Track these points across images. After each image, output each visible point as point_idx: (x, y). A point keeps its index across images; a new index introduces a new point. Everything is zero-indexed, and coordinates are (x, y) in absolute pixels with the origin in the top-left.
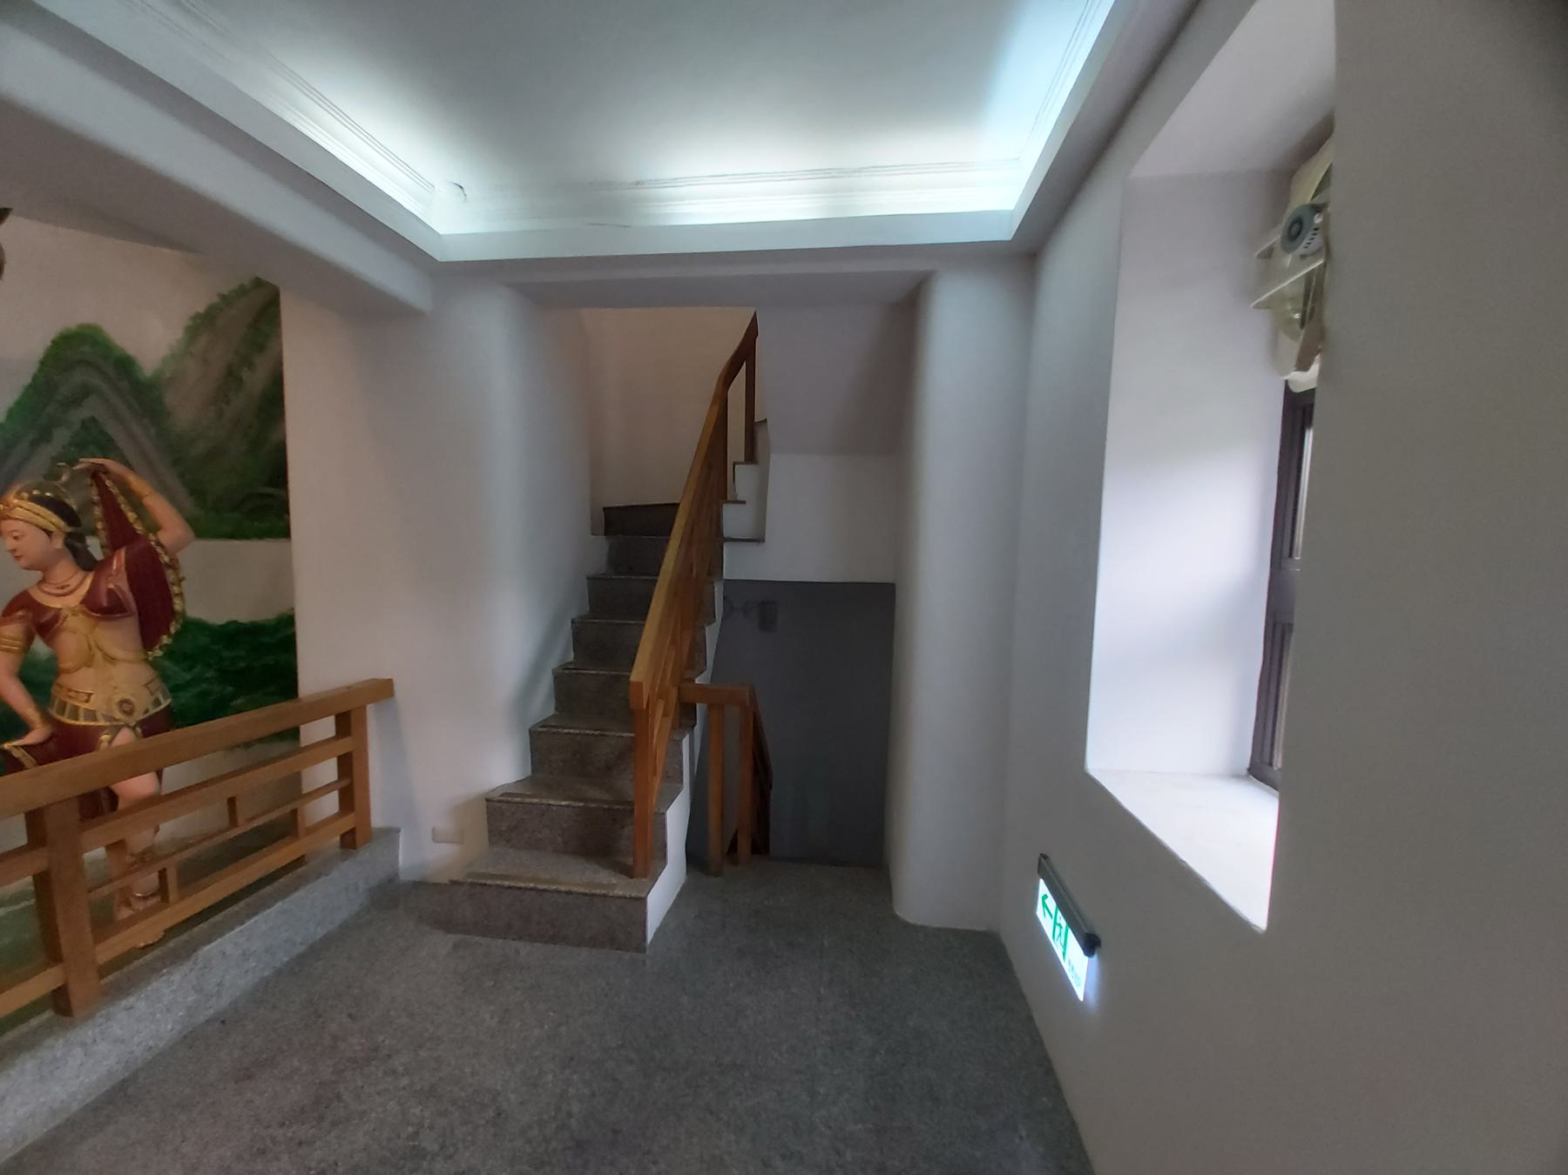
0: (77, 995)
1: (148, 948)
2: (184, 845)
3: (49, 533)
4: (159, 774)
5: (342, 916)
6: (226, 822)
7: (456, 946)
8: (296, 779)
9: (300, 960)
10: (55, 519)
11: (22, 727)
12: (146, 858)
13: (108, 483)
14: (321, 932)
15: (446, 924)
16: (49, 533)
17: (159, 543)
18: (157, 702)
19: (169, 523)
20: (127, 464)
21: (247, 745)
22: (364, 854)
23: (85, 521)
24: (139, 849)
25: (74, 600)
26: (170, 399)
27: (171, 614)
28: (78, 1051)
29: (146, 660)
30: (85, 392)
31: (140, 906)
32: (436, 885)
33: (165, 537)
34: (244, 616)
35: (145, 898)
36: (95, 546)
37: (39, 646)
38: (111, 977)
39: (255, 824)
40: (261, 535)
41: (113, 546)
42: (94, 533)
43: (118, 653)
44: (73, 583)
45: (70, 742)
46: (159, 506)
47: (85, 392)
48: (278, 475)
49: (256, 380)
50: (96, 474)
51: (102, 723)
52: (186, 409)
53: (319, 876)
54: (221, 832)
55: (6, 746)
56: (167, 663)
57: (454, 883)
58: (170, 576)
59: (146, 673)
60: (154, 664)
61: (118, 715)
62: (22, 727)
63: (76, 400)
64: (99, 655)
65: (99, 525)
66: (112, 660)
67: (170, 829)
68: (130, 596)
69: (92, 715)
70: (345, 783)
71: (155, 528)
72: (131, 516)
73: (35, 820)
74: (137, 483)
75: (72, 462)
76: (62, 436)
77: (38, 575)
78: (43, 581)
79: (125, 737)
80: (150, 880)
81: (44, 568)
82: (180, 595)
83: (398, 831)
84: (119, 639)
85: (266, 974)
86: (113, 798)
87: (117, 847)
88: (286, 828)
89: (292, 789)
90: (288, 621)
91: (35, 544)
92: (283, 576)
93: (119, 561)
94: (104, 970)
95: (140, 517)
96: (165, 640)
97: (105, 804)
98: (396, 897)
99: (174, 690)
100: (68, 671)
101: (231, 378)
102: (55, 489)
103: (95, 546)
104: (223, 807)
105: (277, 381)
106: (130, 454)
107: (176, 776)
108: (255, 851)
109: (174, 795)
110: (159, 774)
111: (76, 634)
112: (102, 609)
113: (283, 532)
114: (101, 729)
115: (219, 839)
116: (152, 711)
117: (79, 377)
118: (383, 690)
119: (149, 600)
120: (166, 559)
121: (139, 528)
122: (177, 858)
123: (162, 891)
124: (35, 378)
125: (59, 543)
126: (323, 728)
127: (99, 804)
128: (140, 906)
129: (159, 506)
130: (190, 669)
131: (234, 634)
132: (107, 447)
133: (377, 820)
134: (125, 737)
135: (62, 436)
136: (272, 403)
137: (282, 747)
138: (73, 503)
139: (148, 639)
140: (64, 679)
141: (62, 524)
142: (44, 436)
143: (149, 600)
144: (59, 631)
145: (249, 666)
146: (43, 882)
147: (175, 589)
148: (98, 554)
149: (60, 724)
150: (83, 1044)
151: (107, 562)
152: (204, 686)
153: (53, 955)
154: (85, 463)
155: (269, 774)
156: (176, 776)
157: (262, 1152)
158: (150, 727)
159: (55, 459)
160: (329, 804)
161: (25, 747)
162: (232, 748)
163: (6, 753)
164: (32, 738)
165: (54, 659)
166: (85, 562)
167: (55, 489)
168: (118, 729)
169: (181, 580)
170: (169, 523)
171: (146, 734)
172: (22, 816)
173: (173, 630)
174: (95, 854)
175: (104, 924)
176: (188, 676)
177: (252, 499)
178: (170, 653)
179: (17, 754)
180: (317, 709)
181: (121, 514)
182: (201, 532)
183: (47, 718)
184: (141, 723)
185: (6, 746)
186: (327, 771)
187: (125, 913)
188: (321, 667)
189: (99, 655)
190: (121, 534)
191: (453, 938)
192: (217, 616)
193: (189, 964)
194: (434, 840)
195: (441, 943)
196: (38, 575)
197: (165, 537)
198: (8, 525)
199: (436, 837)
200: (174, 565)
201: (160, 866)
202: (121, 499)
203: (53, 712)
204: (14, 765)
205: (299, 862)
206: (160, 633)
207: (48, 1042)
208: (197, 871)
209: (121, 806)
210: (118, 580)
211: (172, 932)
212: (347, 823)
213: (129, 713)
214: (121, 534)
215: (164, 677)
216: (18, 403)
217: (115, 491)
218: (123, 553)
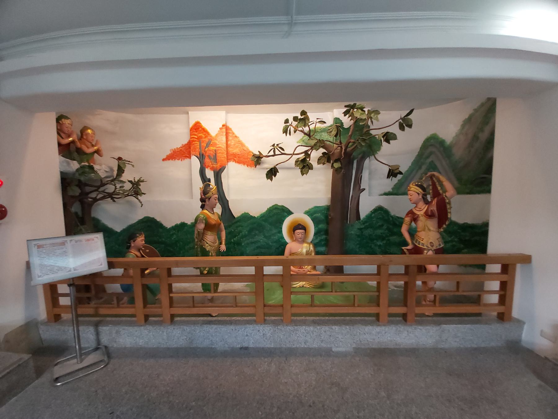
0: (409, 317)
1: (428, 316)
2: (441, 291)
3: (418, 194)
4: (438, 266)
5: (493, 344)
6: (455, 289)
7: (540, 386)
8: (482, 285)
9: (476, 349)
10: (420, 190)
11: (406, 244)
12: (431, 290)
13: (434, 179)
14: (483, 345)
15: (539, 376)
16: (418, 194)
17: (446, 196)
18: (440, 245)
19: (449, 188)
20: (440, 173)
21: (466, 266)
22: (507, 325)
23: (427, 190)
24: (430, 287)
25: (422, 213)
26: (454, 150)
27: (446, 218)
28: (406, 332)
29: (438, 232)
30: (431, 153)
31: (428, 303)
32: (537, 355)
33: (448, 194)
34: (470, 222)
35: (430, 301)
36: (429, 198)
37: (413, 224)
38: (418, 318)
39: (465, 294)
40: (479, 192)
41: (433, 197)
42: (429, 194)
43: (432, 229)
44: (423, 207)
45: (417, 251)
46: (448, 185)
47: (431, 153)
48: (489, 170)
49: (484, 136)
50: (432, 177)
51: (425, 247)
52: (458, 153)
53: (486, 324)
54: (451, 291)
55: (403, 248)
56: (444, 234)
57: (546, 358)
58: (448, 206)
59: (437, 236)
60: (440, 233)
61: (430, 246)
62: (406, 244)
63: (428, 157)
64: (427, 228)
65: (431, 191)
66: (429, 230)
67: (439, 284)
68: (436, 211)
69: (423, 245)
70: (502, 293)
71: (445, 191)
72: (439, 188)
73: (407, 267)
74: (442, 178)
75: (426, 174)
76: (424, 168)
77: (415, 205)
78: (416, 207)
79: (430, 253)
80: (431, 297)
81: (416, 203)
82: (450, 212)
83: (524, 323)
84: (432, 224)
85: (461, 346)
86: (425, 269)
87: (424, 283)
88: (477, 300)
89: (480, 287)
90: (486, 225)
91: (415, 197)
92: (486, 208)
93: (434, 202)
94: (417, 315)
95: (442, 189)
96: (444, 226)
97: (423, 270)
98: (516, 349)
99: (445, 242)
100: (419, 232)
101: (476, 137)
102: (421, 182)
103: (429, 198)
104: (455, 284)
105: (492, 134)
106: (441, 171)
107: (443, 269)
108: (463, 304)
109: (442, 275)
110: (438, 266)
111: (423, 221)
112: (429, 215)
113: (489, 191)
114: (425, 249)
115: (452, 294)
116: (438, 247)
117: (431, 149)
118: (526, 259)
119: (441, 214)
120: (447, 201)
121: (441, 191)
122: (440, 293)
123: (434, 301)
124: (419, 152)
125: (421, 197)
126: (496, 268)
127: (422, 269)
128: (428, 303)
129: (448, 185)
130: (451, 237)
131: (466, 227)
132: (435, 168)
133: (516, 313)
134: (430, 253)
135: (424, 168)
136: (490, 143)
137: (477, 270)
138: (425, 186)
139: (440, 226)
140: (417, 233)
141: (422, 191)
142: (420, 168)
143: (441, 214)
144: (418, 220)
145: (471, 239)
146: (406, 283)
147: (449, 211)
148: (430, 200)
149: (416, 245)
150: (408, 331)
151: (432, 202)
152: (454, 243)
153: (405, 305)
154: (429, 173)
155: (474, 278)
156: (443, 269)
157: (450, 401)
158: (438, 251)
159: (422, 174)
160: (494, 299)
161: (407, 249)
162: (460, 265)
163: (403, 250)
164: (409, 247)
165: (416, 228)
166: (426, 202)
167: (421, 182)
168: (429, 250)
169: (451, 208)
170: (449, 188)
171: (436, 253)
172: (404, 267)
173: (447, 223)
174: (419, 283)
175: (418, 303)
176: (450, 239)
177: (479, 179)
178: (445, 231)
179: (405, 251)
180: (495, 260)
181: (436, 188)
182: (459, 192)
183: (413, 243)
184: (435, 250)
185: (403, 248)
186: (495, 285)
187: (424, 303)
188: (497, 244)
189: (427, 228)
190: (436, 194)
191: (539, 382)
192: (461, 221)
193: (438, 328)
194: (541, 335)
195: (536, 382)
196: (415, 205)
197: (448, 194)
198: (409, 192)
199: (542, 334)
200: (449, 203)
201: (436, 294)
202: (437, 183)
203: (414, 242)
204: (403, 253)
205: (479, 315)
206: (443, 224)
207: (400, 325)
208: (445, 301)
209: (427, 272)
210: (434, 207)
211: (436, 315)
212: (501, 309)
213: (432, 246)
214: (436, 194)
215: (443, 238)
216: (21, 326)
217: (436, 181)
218: (436, 199)
